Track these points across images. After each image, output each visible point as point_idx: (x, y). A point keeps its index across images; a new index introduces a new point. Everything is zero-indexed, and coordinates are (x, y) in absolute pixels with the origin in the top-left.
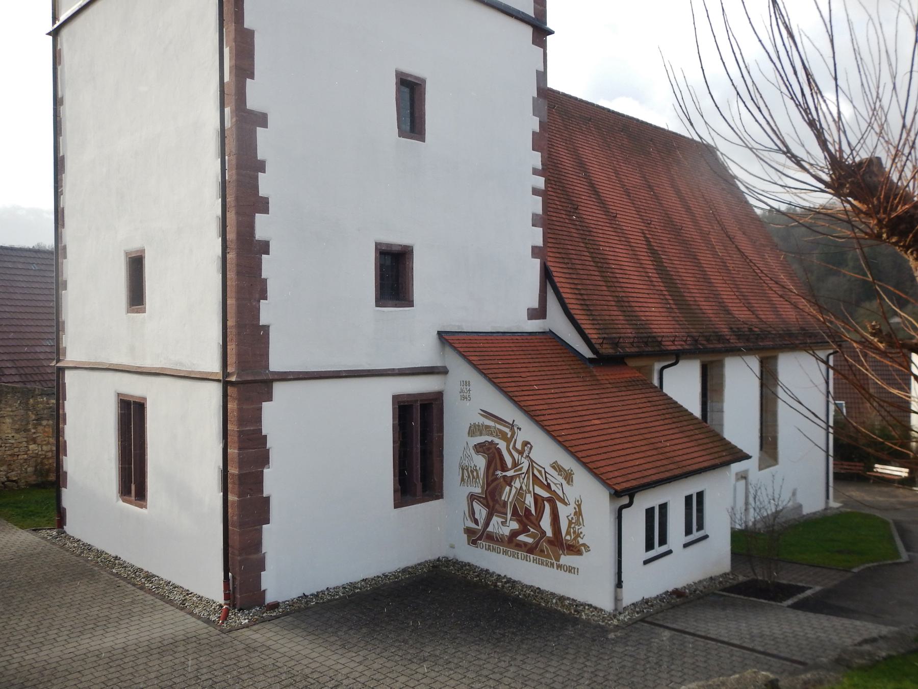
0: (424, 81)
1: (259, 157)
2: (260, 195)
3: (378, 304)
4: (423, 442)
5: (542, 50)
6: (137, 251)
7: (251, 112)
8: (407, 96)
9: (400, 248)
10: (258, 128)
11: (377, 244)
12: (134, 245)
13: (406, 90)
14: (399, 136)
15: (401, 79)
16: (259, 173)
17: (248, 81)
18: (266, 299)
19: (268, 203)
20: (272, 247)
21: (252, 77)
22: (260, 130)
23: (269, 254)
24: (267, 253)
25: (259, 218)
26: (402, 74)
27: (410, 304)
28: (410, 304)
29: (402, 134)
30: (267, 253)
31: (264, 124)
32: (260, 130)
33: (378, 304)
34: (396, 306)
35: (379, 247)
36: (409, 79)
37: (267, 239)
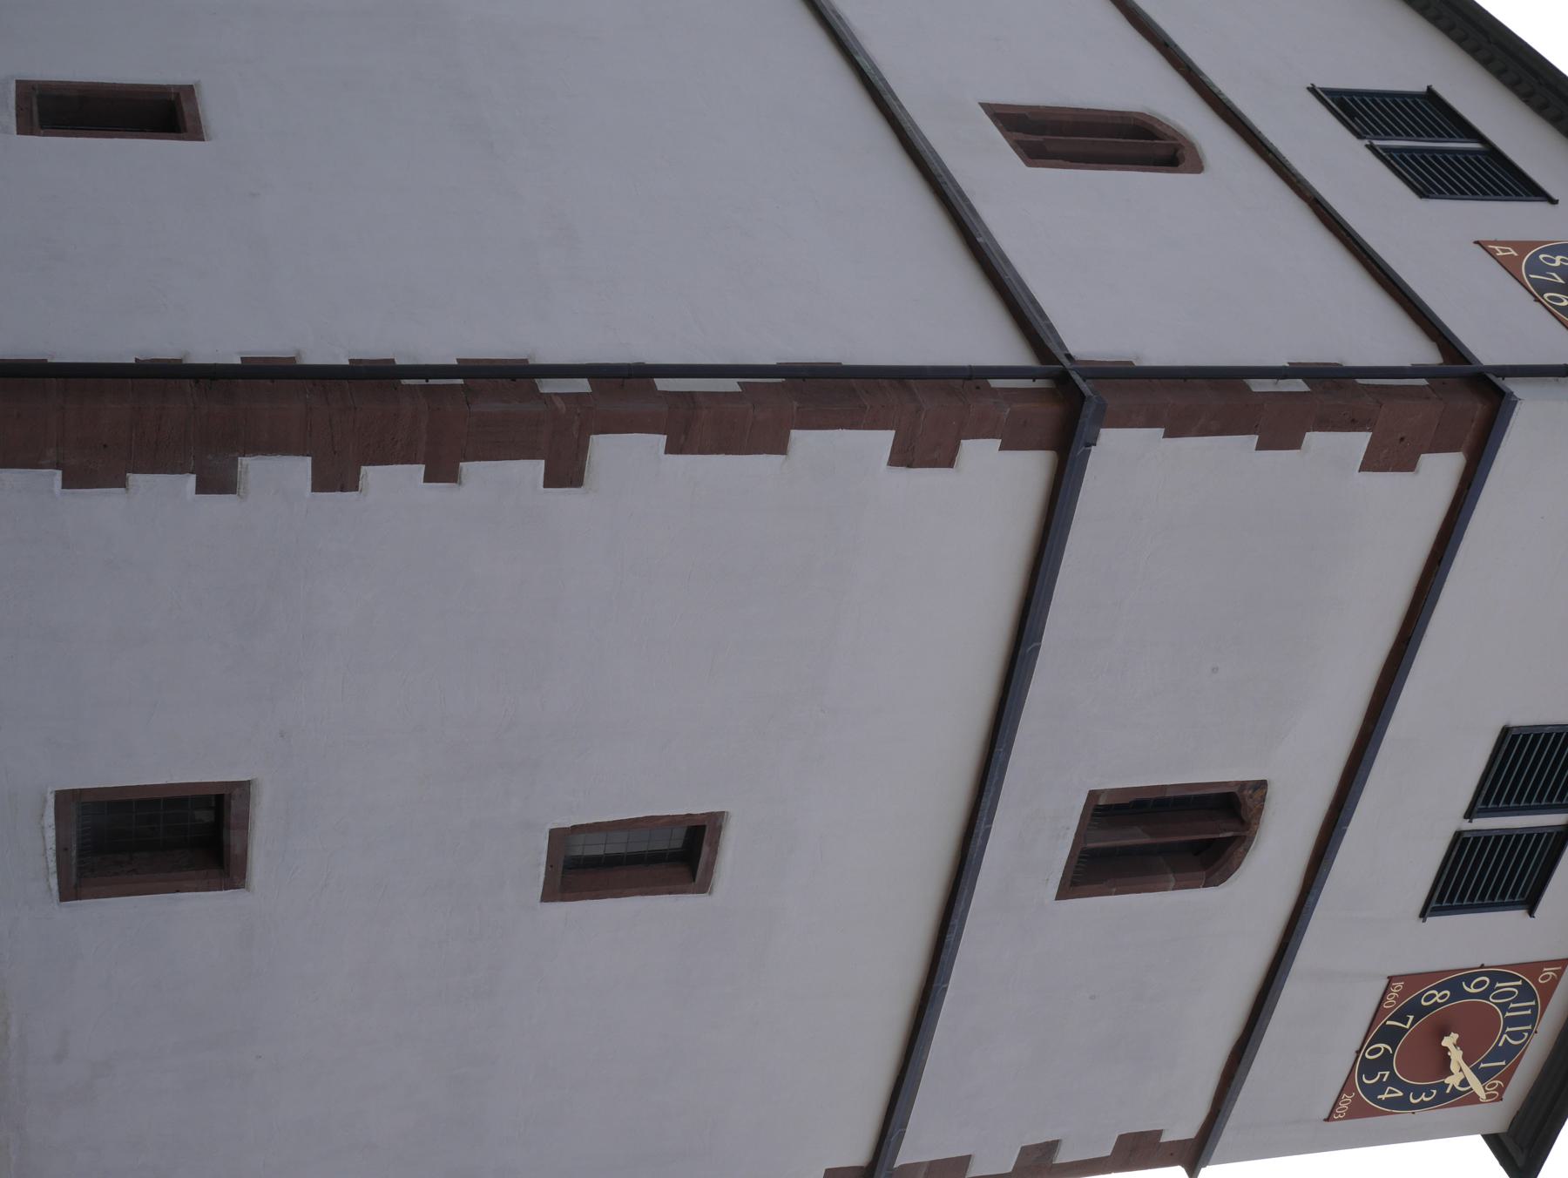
0: (704, 888)
1: (466, 467)
2: (364, 469)
3: (65, 799)
4: (1451, 854)
5: (1108, 1152)
6: (197, 119)
7: (582, 450)
8: (660, 844)
9: (236, 850)
10: (542, 463)
11: (244, 787)
12: (211, 109)
13: (676, 841)
14: (552, 832)
15: (704, 826)
16: (894, 432)
17: (662, 439)
18: (67, 484)
19: (342, 490)
20: (440, 490)
21: (670, 449)
22: (884, 439)
23: (425, 481)
24: (202, 488)
25: (300, 468)
26: (718, 830)
27: (69, 892)
28: (69, 892)
29: (559, 838)
30: (202, 488)
31: (552, 480)
32: (884, 439)
33: (65, 799)
34: (61, 850)
35: (237, 792)
36: (705, 849)
37: (241, 488)
